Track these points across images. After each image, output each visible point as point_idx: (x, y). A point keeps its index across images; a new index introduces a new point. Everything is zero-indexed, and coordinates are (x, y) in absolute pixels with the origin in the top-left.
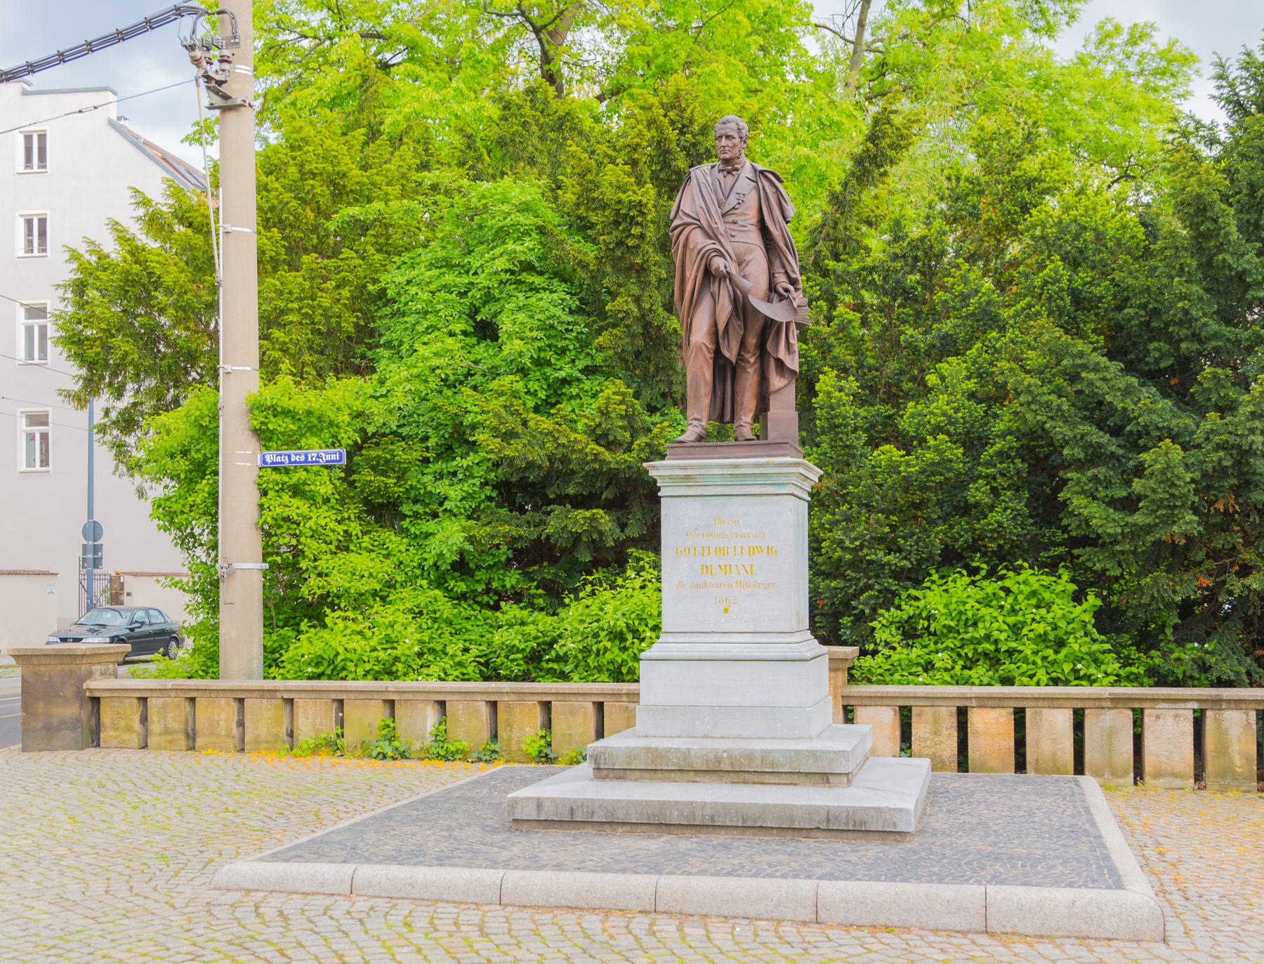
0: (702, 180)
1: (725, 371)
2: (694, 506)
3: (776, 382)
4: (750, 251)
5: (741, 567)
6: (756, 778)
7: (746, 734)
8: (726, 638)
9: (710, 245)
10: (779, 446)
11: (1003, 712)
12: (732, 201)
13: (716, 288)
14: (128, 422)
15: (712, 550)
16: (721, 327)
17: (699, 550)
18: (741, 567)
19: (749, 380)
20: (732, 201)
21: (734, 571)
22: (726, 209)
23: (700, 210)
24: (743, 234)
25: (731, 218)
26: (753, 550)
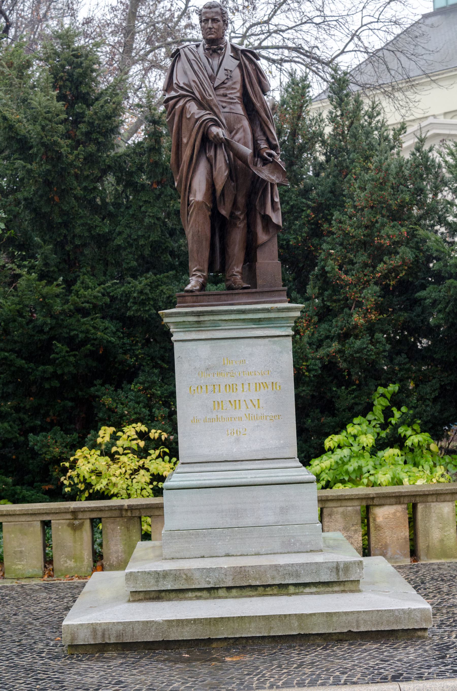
0: (191, 57)
1: (220, 226)
2: (203, 350)
3: (262, 237)
7: (263, 551)
9: (206, 115)
10: (270, 293)
11: (399, 508)
12: (221, 76)
13: (212, 153)
15: (222, 388)
16: (219, 187)
17: (210, 388)
19: (237, 237)
20: (221, 76)
21: (243, 404)
25: (221, 92)
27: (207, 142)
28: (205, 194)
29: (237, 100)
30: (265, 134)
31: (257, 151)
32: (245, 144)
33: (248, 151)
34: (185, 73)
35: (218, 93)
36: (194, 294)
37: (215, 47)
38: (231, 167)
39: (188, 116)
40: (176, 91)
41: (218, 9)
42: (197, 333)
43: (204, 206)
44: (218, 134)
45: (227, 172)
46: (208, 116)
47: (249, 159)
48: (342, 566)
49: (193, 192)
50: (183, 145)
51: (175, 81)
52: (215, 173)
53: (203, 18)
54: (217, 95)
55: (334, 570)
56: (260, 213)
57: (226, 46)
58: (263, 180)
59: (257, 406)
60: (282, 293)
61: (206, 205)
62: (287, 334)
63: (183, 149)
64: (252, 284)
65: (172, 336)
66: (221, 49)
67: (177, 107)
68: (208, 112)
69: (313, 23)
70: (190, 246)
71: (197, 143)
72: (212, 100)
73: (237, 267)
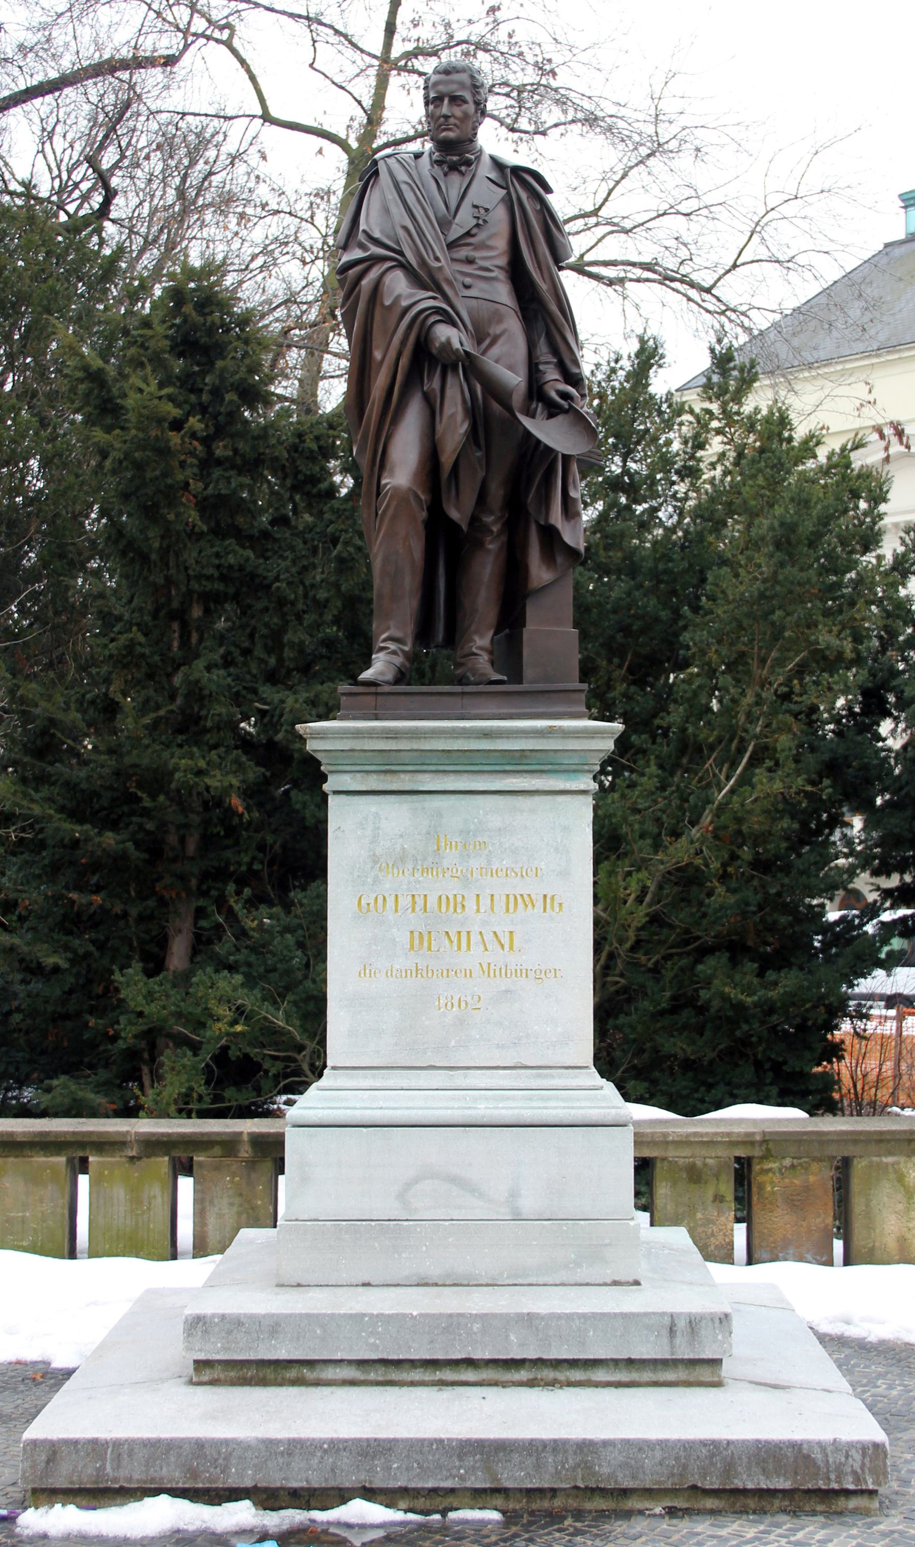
0: (402, 176)
1: (446, 545)
2: (393, 819)
3: (539, 573)
4: (498, 318)
5: (489, 937)
6: (577, 1375)
8: (459, 1078)
9: (426, 300)
10: (545, 698)
12: (465, 219)
13: (436, 384)
14: (105, 408)
16: (447, 458)
18: (489, 937)
19: (486, 570)
20: (465, 219)
22: (455, 232)
23: (401, 233)
24: (483, 285)
25: (463, 253)
26: (513, 902)
27: (424, 358)
28: (416, 475)
29: (496, 273)
30: (555, 352)
31: (535, 390)
32: (511, 368)
33: (514, 379)
34: (386, 211)
35: (456, 256)
36: (380, 690)
37: (455, 158)
38: (477, 416)
39: (387, 303)
40: (362, 247)
41: (464, 77)
42: (382, 777)
43: (412, 499)
44: (449, 342)
45: (466, 426)
46: (431, 303)
47: (517, 399)
48: (682, 1324)
49: (388, 467)
50: (374, 366)
51: (363, 226)
52: (440, 428)
53: (432, 95)
54: (453, 260)
55: (665, 1332)
56: (537, 523)
57: (478, 158)
58: (549, 450)
59: (507, 947)
60: (575, 696)
61: (417, 496)
62: (582, 787)
63: (373, 374)
64: (512, 679)
65: (325, 780)
66: (468, 163)
67: (364, 282)
68: (430, 294)
69: (678, 213)
70: (376, 583)
71: (404, 362)
72: (440, 269)
73: (482, 636)
